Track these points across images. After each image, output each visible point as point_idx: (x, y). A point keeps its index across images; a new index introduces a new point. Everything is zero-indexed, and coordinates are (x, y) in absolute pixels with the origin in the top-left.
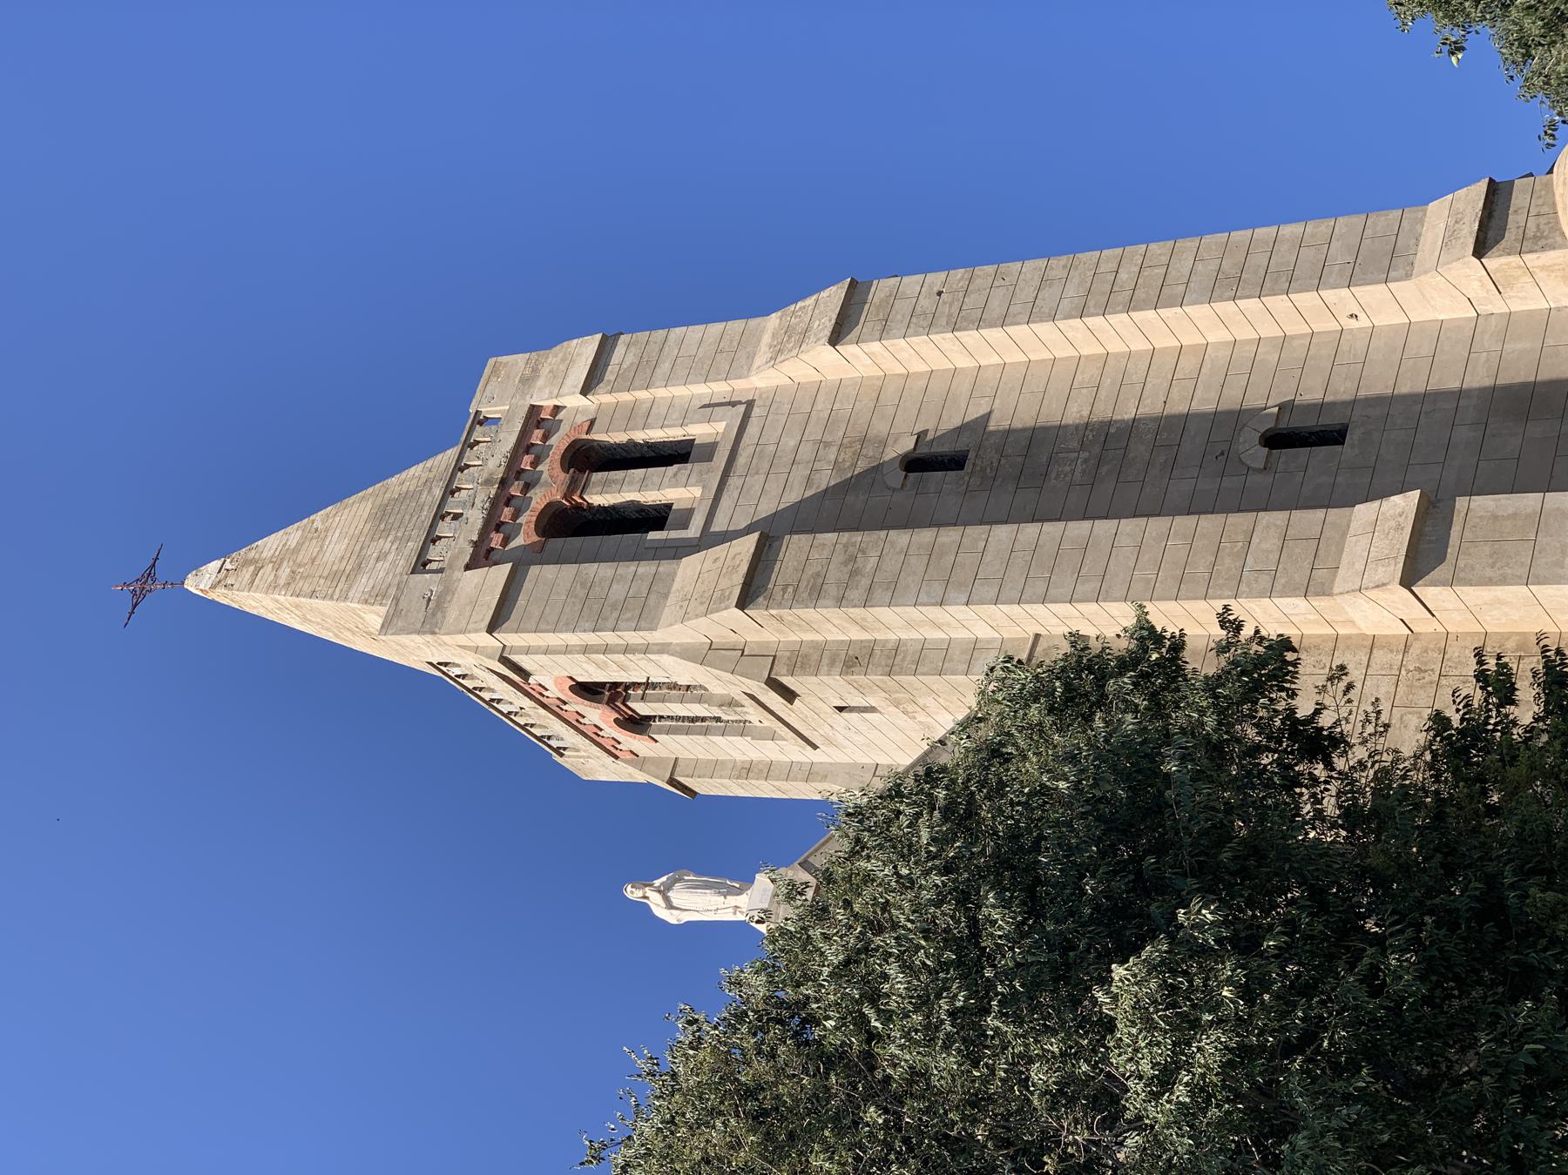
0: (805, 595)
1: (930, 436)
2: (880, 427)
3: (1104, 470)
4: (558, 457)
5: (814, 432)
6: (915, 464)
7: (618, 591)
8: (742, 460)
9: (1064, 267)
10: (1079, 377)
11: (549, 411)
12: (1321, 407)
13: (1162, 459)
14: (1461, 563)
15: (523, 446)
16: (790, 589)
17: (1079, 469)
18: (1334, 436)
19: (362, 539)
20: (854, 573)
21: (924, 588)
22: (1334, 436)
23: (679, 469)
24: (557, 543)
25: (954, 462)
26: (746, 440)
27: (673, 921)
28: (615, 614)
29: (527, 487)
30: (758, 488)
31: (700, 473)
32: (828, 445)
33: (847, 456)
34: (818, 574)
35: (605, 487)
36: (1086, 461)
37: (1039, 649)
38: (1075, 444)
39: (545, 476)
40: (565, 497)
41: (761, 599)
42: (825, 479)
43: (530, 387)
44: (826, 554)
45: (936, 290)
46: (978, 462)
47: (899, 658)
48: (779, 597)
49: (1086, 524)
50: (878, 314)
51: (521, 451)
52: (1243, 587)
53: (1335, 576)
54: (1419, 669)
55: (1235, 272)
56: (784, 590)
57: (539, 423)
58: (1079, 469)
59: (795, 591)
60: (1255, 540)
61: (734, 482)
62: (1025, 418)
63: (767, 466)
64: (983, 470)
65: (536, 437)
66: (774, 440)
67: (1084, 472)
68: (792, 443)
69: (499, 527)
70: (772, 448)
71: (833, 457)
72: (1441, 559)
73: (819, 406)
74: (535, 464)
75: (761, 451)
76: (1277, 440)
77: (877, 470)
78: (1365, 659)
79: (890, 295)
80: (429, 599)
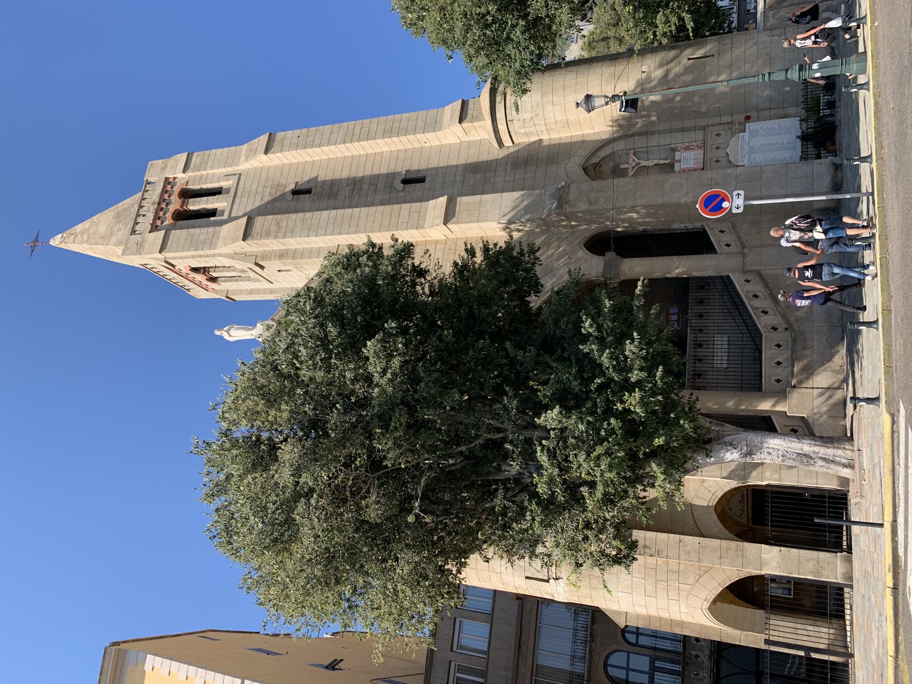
1: (300, 183)
3: (355, 192)
5: (262, 183)
6: (296, 192)
7: (202, 238)
8: (239, 193)
15: (164, 191)
18: (422, 180)
20: (279, 228)
22: (422, 180)
25: (308, 191)
29: (167, 204)
32: (267, 187)
33: (273, 190)
38: (345, 185)
42: (267, 198)
58: (347, 192)
61: (237, 200)
68: (255, 187)
72: (454, 216)
74: (169, 197)
76: (406, 182)
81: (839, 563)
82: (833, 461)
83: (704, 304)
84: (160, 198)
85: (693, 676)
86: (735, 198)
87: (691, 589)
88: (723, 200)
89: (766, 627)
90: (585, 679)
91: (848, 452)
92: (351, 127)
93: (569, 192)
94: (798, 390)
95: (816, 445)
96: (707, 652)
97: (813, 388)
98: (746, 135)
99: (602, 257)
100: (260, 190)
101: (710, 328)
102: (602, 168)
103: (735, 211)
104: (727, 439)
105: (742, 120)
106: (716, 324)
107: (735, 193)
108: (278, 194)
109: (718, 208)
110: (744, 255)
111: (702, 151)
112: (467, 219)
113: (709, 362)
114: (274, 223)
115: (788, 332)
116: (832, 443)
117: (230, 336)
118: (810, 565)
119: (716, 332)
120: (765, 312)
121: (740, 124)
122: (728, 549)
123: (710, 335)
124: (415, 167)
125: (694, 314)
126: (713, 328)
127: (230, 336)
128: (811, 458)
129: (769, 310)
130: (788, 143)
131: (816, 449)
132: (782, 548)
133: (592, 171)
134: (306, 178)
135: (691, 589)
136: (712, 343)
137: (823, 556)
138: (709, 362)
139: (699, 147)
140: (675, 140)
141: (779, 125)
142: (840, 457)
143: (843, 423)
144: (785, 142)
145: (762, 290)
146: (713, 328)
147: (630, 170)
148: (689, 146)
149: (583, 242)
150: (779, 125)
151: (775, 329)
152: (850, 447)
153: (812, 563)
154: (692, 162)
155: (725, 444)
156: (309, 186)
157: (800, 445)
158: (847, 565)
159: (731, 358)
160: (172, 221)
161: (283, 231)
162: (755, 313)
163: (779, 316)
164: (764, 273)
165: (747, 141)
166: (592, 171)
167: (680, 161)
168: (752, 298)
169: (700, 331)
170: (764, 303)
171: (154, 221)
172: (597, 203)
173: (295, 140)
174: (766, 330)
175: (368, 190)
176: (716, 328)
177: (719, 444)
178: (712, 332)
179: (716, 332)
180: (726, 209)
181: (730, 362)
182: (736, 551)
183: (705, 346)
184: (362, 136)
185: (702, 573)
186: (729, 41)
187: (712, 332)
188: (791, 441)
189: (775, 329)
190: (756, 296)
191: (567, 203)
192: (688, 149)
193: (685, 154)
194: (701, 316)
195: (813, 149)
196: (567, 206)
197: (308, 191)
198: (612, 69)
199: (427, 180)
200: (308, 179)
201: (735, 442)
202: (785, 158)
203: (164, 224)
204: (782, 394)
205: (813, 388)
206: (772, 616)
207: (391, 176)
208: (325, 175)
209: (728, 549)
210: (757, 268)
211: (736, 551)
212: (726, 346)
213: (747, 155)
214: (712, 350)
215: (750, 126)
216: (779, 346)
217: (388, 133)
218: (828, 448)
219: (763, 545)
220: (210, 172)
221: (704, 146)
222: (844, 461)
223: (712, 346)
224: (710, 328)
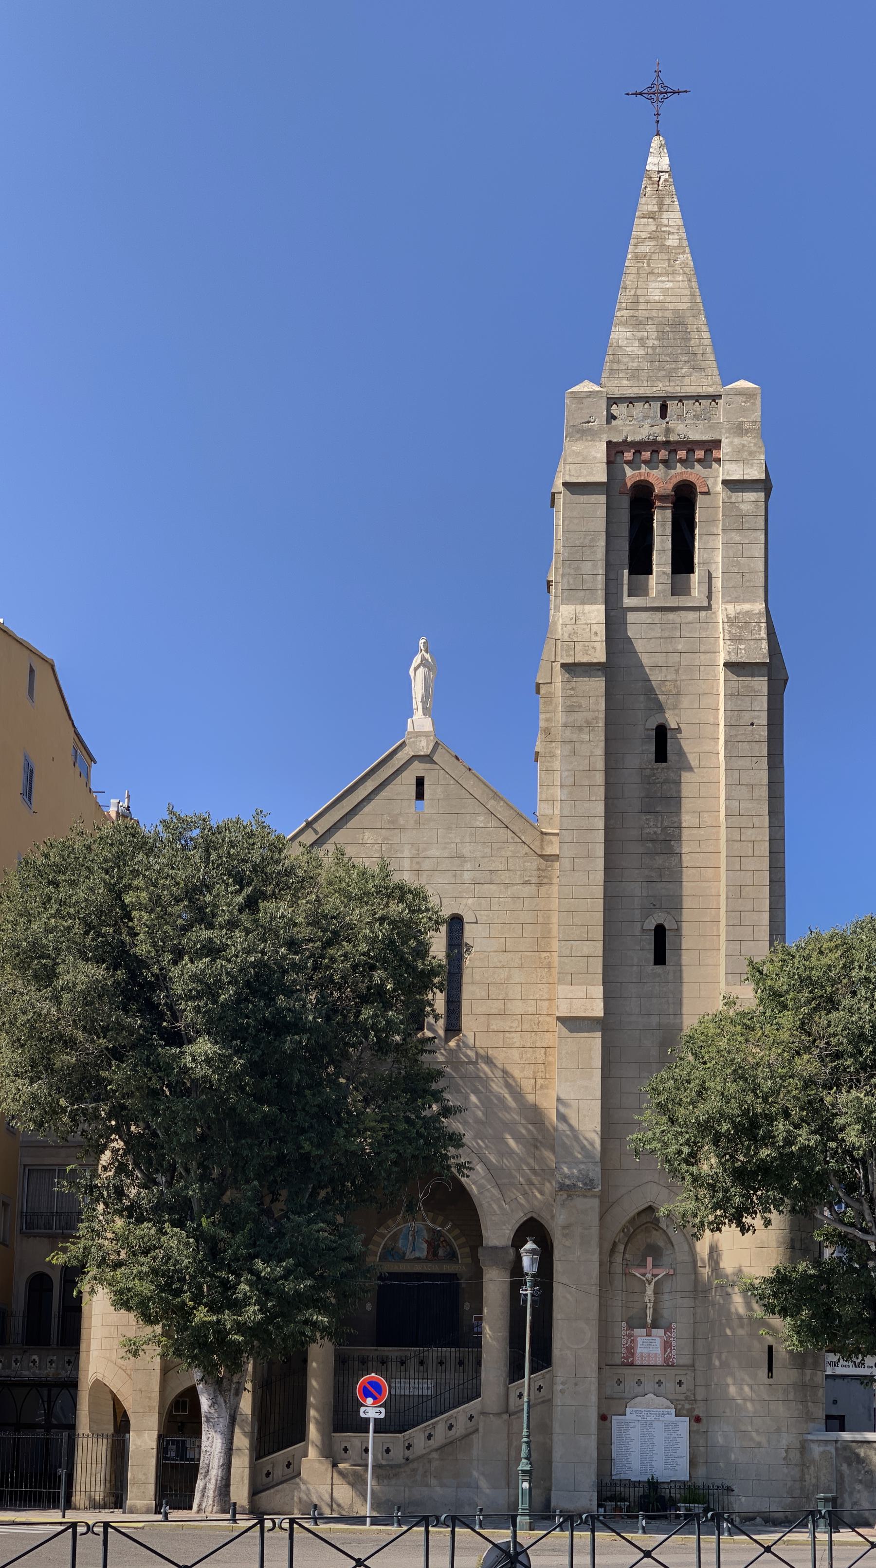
0: (569, 703)
1: (679, 736)
2: (685, 702)
3: (650, 845)
4: (685, 477)
5: (686, 659)
6: (662, 734)
7: (587, 567)
8: (671, 616)
9: (760, 796)
10: (706, 815)
11: (717, 456)
12: (679, 949)
13: (653, 874)
14: (569, 1040)
15: (691, 446)
16: (572, 692)
17: (651, 831)
18: (660, 958)
19: (654, 314)
20: (580, 729)
21: (570, 773)
22: (660, 958)
23: (667, 575)
24: (625, 502)
25: (661, 755)
26: (683, 614)
27: (586, 382)
28: (572, 572)
29: (665, 462)
30: (653, 634)
31: (664, 591)
32: (677, 671)
33: (669, 686)
34: (580, 706)
35: (663, 523)
36: (655, 833)
37: (551, 837)
38: (665, 823)
39: (673, 472)
40: (656, 495)
41: (567, 675)
42: (655, 677)
43: (735, 433)
44: (593, 707)
45: (755, 721)
46: (659, 770)
47: (549, 759)
48: (569, 687)
49: (602, 854)
50: (743, 687)
51: (689, 446)
52: (563, 943)
53: (568, 984)
54: (539, 1022)
55: (743, 894)
56: (574, 689)
57: (709, 451)
58: (651, 831)
59: (571, 696)
60: (588, 943)
61: (657, 616)
62: (686, 790)
63: (666, 635)
64: (654, 775)
65: (700, 454)
66: (684, 633)
67: (650, 833)
68: (680, 647)
69: (638, 452)
70: (678, 634)
71: (669, 678)
72: (571, 1031)
73: (703, 656)
74: (681, 461)
75: (676, 628)
76: (660, 932)
77: (660, 708)
78: (544, 998)
79: (755, 691)
80: (589, 422)
81: (145, 1502)
82: (203, 1495)
83: (458, 1366)
84: (677, 442)
85: (66, 1359)
86: (377, 1409)
87: (112, 1362)
88: (375, 1398)
89: (97, 1435)
90: (65, 1231)
91: (210, 1509)
92: (757, 822)
93: (585, 1196)
94: (330, 1469)
95: (217, 1481)
96: (63, 1374)
97: (332, 1484)
98: (672, 1417)
99: (510, 1243)
100: (674, 658)
101: (443, 1374)
102: (655, 1232)
103: (362, 1409)
104: (220, 1399)
105: (696, 1413)
106: (448, 1381)
107: (383, 1410)
108: (662, 698)
109: (367, 1394)
110: (498, 1415)
111: (660, 1361)
112: (564, 1052)
113: (398, 1374)
114: (589, 715)
115: (404, 1461)
116: (220, 1495)
117: (416, 670)
118: (141, 1476)
119: (439, 1381)
120: (429, 1437)
121: (691, 1410)
122: (150, 1398)
123: (434, 1374)
124: (687, 943)
125: (462, 1355)
126: (443, 1378)
127: (416, 670)
128: (206, 1476)
129: (431, 1442)
130: (652, 1467)
131: (213, 1481)
132: (155, 1451)
133: (644, 1218)
134: (686, 746)
135: (112, 1362)
136: (425, 1376)
137: (151, 1488)
138: (398, 1374)
139: (666, 1360)
140: (681, 1330)
141: (681, 1457)
142: (207, 1502)
143: (296, 1511)
144: (654, 1463)
145: (458, 1434)
146: (443, 1378)
147: (642, 1271)
148: (670, 1346)
149: (535, 1216)
150: (681, 1457)
151: (409, 1447)
152: (215, 1510)
153: (143, 1478)
154: (645, 1351)
155: (215, 1397)
156: (670, 756)
157: (216, 1467)
158: (144, 1509)
159: (402, 1399)
160: (629, 484)
161: (575, 737)
162: (429, 1426)
163: (424, 1452)
164: (474, 1436)
165: (661, 1419)
166: (644, 1218)
167: (649, 1335)
168: (449, 1422)
169: (422, 1363)
170: (441, 1434)
171: (633, 444)
172: (565, 1236)
173: (747, 718)
174: (407, 1437)
175: (651, 868)
176: (443, 1381)
177: (215, 1392)
178: (439, 1377)
179: (439, 1381)
180: (365, 1401)
181: (398, 1398)
182: (149, 1406)
183: (421, 1368)
184: (737, 845)
185: (129, 1372)
186: (791, 1396)
187: (439, 1377)
188: (219, 1459)
189: (409, 1447)
190: (451, 1427)
191: (569, 1196)
192: (667, 1345)
193: (658, 1342)
194: (461, 1363)
195: (637, 1494)
196: (565, 1196)
197: (661, 755)
198: (774, 1244)
199: (659, 969)
200: (686, 749)
201: (216, 1407)
202: (630, 1463)
203: (626, 468)
204: (332, 1456)
205: (332, 1484)
206: (110, 1441)
207: (674, 905)
208: (689, 784)
209: (150, 1398)
210: (481, 1430)
211: (149, 1406)
212: (416, 1393)
213: (640, 1418)
214: (412, 1376)
215: (684, 1424)
216: (388, 1451)
217: (736, 892)
218: (215, 1491)
219: (156, 1433)
220: (719, 542)
221: (668, 1364)
222: (204, 1505)
223: (416, 1376)
224: (443, 1374)
